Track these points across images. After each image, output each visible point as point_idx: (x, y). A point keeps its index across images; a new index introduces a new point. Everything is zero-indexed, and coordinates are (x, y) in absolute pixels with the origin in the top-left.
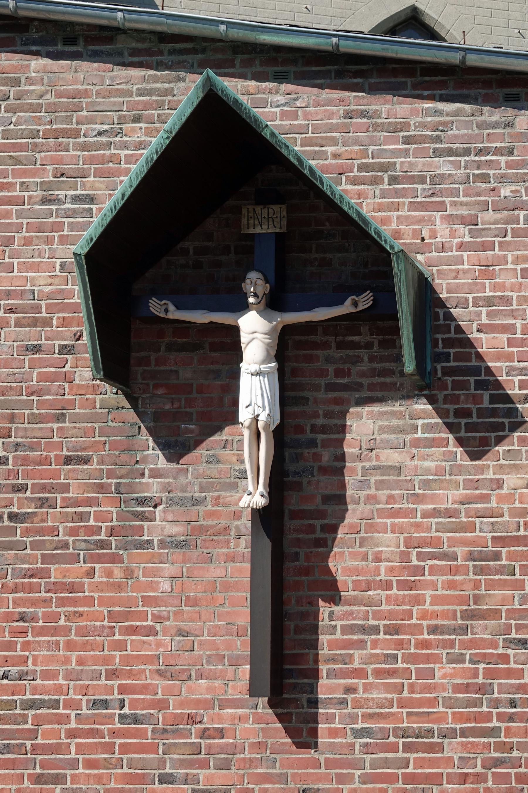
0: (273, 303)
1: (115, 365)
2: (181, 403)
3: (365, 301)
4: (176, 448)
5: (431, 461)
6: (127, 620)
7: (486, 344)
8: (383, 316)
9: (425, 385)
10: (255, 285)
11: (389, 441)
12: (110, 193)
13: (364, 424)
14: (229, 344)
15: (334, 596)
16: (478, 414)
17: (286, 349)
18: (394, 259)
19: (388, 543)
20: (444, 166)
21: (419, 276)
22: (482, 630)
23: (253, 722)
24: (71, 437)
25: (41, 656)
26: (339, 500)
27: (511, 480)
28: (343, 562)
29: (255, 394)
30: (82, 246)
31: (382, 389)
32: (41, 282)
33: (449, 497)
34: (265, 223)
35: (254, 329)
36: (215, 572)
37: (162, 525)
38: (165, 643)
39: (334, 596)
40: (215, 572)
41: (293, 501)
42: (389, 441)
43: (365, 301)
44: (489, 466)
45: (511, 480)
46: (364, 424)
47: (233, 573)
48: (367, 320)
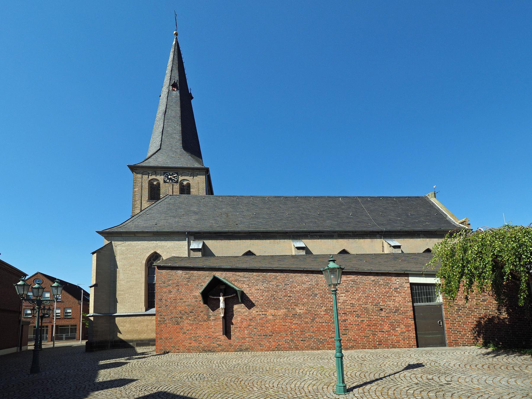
0: (223, 296)
1: (205, 302)
2: (215, 306)
3: (235, 295)
4: (213, 310)
5: (244, 310)
6: (208, 328)
7: (250, 298)
8: (237, 295)
9: (243, 302)
10: (221, 294)
11: (239, 309)
12: (205, 285)
13: (236, 307)
14: (219, 300)
15: (233, 324)
16: (250, 305)
17: (225, 301)
18: (406, 278)
19: (239, 319)
20: (244, 279)
21: (151, 187)
22: (250, 327)
23: (224, 337)
24: (201, 310)
25: (199, 331)
26: (233, 315)
27: (254, 312)
28: (233, 321)
29: (222, 305)
30: (201, 291)
31: (238, 303)
32: (197, 294)
33: (246, 314)
34: (223, 287)
35: (221, 298)
36: (218, 322)
37: (212, 318)
38: (213, 330)
39: (233, 324)
40: (218, 322)
41: (227, 315)
42: (239, 309)
43: (235, 295)
44: (251, 310)
45: (254, 312)
46: (236, 307)
47: (220, 322)
48: (236, 297)
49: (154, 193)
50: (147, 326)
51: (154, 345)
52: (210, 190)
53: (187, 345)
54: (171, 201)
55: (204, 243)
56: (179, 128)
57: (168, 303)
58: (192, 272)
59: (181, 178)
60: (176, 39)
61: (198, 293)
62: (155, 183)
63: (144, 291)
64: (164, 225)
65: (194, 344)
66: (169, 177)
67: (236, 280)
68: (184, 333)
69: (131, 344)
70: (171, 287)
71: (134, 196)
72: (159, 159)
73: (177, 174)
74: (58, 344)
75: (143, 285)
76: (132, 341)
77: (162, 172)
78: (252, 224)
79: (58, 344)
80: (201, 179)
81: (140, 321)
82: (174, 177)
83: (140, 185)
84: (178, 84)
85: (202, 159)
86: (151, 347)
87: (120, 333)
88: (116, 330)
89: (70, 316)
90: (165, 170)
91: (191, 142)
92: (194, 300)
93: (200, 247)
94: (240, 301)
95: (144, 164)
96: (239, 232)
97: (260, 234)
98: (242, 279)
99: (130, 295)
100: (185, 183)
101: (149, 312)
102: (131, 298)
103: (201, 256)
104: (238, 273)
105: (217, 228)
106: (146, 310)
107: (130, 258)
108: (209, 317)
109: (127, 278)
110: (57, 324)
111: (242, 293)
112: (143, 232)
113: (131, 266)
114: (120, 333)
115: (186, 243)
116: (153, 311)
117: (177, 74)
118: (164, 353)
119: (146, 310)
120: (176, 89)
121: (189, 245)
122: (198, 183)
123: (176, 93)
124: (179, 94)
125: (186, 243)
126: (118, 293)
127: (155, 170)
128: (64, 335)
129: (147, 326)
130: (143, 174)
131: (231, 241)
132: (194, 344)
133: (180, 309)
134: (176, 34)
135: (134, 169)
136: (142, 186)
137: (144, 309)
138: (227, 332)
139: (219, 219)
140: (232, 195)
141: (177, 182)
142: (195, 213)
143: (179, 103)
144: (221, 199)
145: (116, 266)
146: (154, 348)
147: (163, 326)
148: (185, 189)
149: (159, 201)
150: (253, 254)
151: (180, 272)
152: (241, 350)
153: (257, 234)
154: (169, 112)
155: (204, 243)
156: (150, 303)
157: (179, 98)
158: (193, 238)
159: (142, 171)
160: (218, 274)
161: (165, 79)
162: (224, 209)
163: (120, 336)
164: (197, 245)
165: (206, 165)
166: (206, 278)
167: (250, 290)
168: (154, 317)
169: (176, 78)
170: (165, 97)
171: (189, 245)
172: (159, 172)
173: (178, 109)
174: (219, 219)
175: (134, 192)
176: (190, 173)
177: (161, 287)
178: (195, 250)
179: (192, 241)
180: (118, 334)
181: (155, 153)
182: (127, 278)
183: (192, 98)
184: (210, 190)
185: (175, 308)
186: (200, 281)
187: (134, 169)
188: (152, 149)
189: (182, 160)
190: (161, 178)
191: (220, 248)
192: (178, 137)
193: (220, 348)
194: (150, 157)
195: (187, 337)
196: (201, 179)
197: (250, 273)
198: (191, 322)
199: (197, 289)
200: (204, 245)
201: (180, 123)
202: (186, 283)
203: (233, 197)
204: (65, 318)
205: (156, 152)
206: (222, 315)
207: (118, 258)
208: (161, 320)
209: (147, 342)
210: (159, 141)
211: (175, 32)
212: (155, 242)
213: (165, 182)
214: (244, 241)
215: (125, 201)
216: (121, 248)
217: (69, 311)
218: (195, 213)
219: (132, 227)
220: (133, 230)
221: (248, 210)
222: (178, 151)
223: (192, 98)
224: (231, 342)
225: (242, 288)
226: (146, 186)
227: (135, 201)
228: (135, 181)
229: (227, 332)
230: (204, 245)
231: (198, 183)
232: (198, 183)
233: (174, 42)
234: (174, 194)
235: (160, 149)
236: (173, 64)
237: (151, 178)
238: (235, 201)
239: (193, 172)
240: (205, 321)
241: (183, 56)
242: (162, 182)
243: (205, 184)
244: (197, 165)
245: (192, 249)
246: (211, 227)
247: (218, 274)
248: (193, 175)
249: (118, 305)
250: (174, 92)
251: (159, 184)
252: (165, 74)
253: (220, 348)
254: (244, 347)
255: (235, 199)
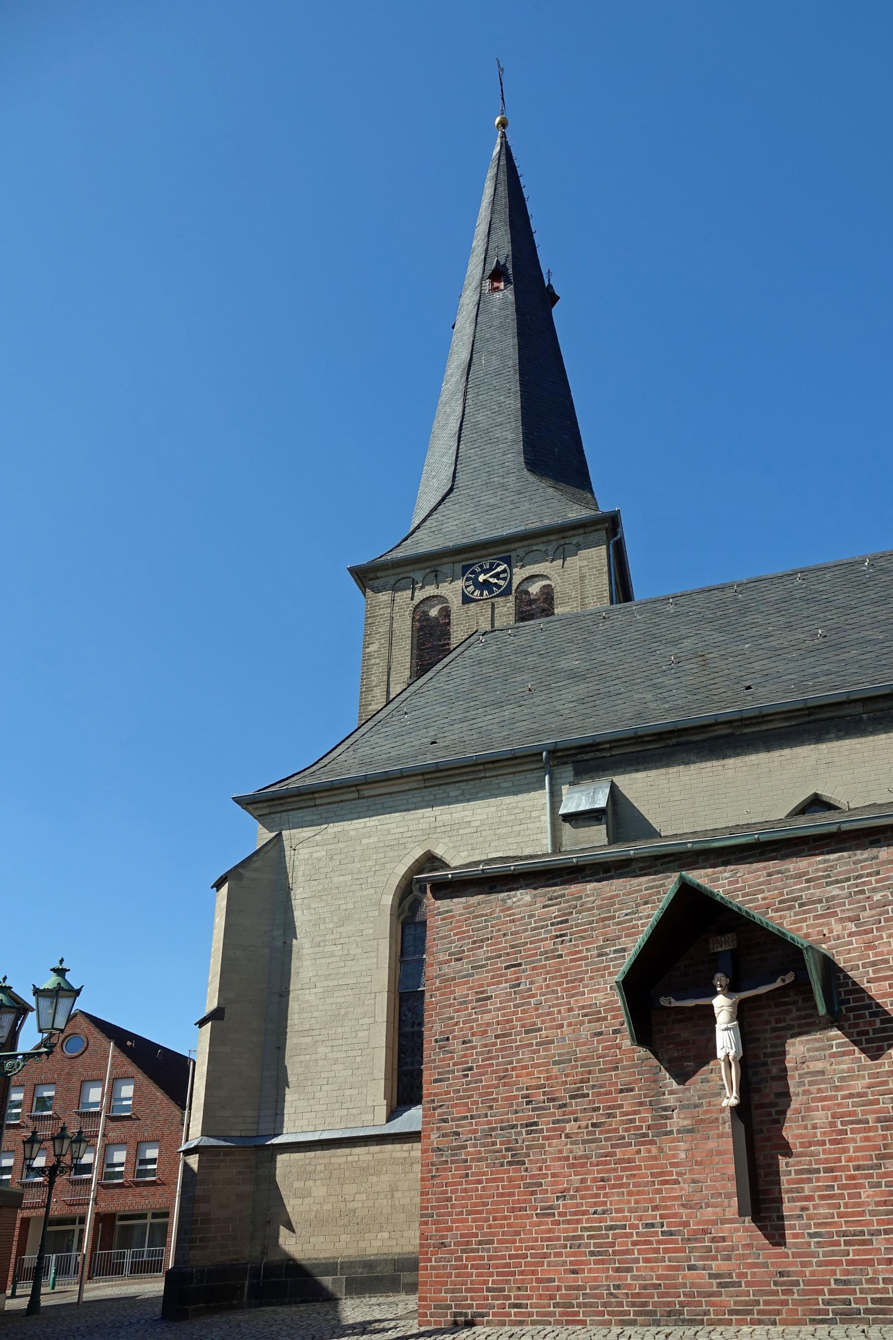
1: (643, 1035)
3: (790, 978)
4: (682, 1077)
7: (873, 989)
8: (802, 985)
9: (835, 1020)
10: (720, 980)
11: (816, 1059)
13: (797, 1049)
17: (743, 1015)
19: (821, 1117)
20: (834, 891)
23: (743, 1232)
24: (621, 1078)
25: (614, 1200)
26: (786, 1095)
28: (791, 1132)
29: (726, 1041)
30: (619, 977)
31: (808, 1024)
32: (600, 998)
33: (859, 1085)
34: (724, 945)
35: (721, 1004)
36: (711, 1145)
37: (677, 1121)
39: (787, 1151)
40: (711, 1145)
41: (756, 1099)
42: (816, 1059)
43: (790, 978)
46: (797, 1049)
48: (792, 987)
49: (431, 643)
50: (393, 1189)
51: (412, 1288)
52: (622, 590)
53: (561, 1277)
54: (487, 654)
55: (613, 788)
56: (514, 403)
57: (475, 1059)
58: (574, 888)
59: (519, 574)
60: (504, 136)
61: (605, 993)
62: (434, 612)
63: (383, 1028)
64: (461, 740)
65: (594, 1274)
66: (481, 578)
67: (787, 904)
68: (547, 1212)
69: (327, 1281)
70: (484, 975)
71: (366, 672)
72: (450, 526)
73: (507, 560)
74: (102, 1289)
75: (383, 1000)
76: (330, 1268)
77: (458, 568)
78: (815, 676)
79: (102, 1289)
80: (594, 559)
81: (365, 1170)
82: (497, 576)
83: (384, 629)
84: (509, 266)
85: (592, 492)
86: (403, 1296)
87: (290, 1228)
88: (270, 1212)
89: (153, 1172)
90: (466, 558)
91: (552, 442)
92: (585, 1031)
93: (601, 802)
94: (822, 1010)
95: (399, 554)
96: (762, 717)
97: (859, 709)
98: (817, 893)
99: (333, 1073)
100: (534, 589)
101: (400, 1125)
102: (336, 1061)
103: (605, 841)
104: (794, 865)
105: (661, 715)
106: (392, 1115)
107: (341, 881)
108: (663, 1113)
109: (327, 977)
110: (106, 1207)
111: (828, 965)
112: (387, 778)
113: (342, 922)
114: (290, 1228)
115: (543, 797)
116: (412, 1119)
117: (508, 237)
118: (455, 1327)
119: (392, 1115)
120: (502, 285)
121: (555, 799)
122: (582, 578)
123: (505, 295)
124: (511, 297)
125: (543, 797)
126: (292, 1041)
127: (433, 565)
128: (128, 1252)
129: (393, 1189)
130: (395, 589)
131: (730, 762)
132: (594, 1274)
133: (525, 1081)
134: (503, 124)
135: (367, 576)
136: (391, 632)
137: (382, 1112)
138: (762, 1202)
139: (668, 681)
140: (716, 583)
141: (506, 592)
142: (575, 676)
143: (514, 324)
144: (671, 609)
145: (289, 929)
146: (411, 1302)
147: (450, 1176)
148: (535, 608)
149: (446, 660)
150: (829, 807)
151: (523, 897)
152: (848, 1316)
153: (846, 711)
154: (481, 360)
155: (613, 788)
156: (406, 1089)
157: (512, 309)
158: (568, 771)
159: (392, 580)
160: (700, 877)
161: (470, 267)
162: (687, 643)
163: (291, 1244)
164: (583, 797)
165: (605, 507)
166: (637, 908)
167: (870, 946)
168: (415, 1150)
169: (504, 249)
170: (473, 319)
171: (555, 799)
172: (446, 569)
173: (509, 344)
174: (668, 681)
175: (367, 657)
176: (551, 548)
177: (447, 980)
178: (576, 818)
179: (565, 789)
180: (283, 1231)
181: (435, 509)
182: (327, 977)
183: (555, 299)
184: (622, 590)
185: (503, 1077)
186: (613, 929)
187: (367, 576)
188: (427, 499)
189: (526, 506)
190: (452, 590)
191: (681, 800)
192: (509, 433)
193: (728, 1300)
194: (418, 527)
195: (562, 1230)
196: (594, 559)
197: (860, 855)
198: (579, 1150)
199: (600, 971)
200: (615, 794)
201: (516, 387)
202: (550, 945)
203: (722, 588)
204: (137, 1184)
205: (443, 499)
206: (731, 1099)
207: (298, 896)
208: (445, 1142)
209: (388, 1271)
210: (452, 467)
211: (498, 120)
212: (427, 812)
213: (467, 600)
214: (786, 752)
215: (338, 679)
216: (311, 850)
217: (152, 1153)
218: (575, 676)
219: (349, 766)
220: (355, 773)
221: (789, 626)
222: (512, 479)
223: (555, 299)
224: (786, 1258)
225: (825, 939)
226: (404, 627)
227: (370, 690)
228: (369, 620)
229: (762, 1202)
230: (615, 794)
231: (578, 578)
232: (582, 578)
233: (498, 149)
234: (497, 624)
235: (451, 490)
236: (492, 212)
237: (420, 595)
238: (727, 606)
239: (560, 539)
240: (643, 1139)
241: (522, 181)
242: (455, 602)
243: (606, 577)
244: (576, 513)
245: (568, 818)
246: (639, 715)
247: (700, 877)
248: (562, 553)
249: (290, 1096)
250: (498, 295)
251: (446, 612)
252: (469, 251)
253: (728, 1300)
254: (862, 1296)
255: (730, 593)
